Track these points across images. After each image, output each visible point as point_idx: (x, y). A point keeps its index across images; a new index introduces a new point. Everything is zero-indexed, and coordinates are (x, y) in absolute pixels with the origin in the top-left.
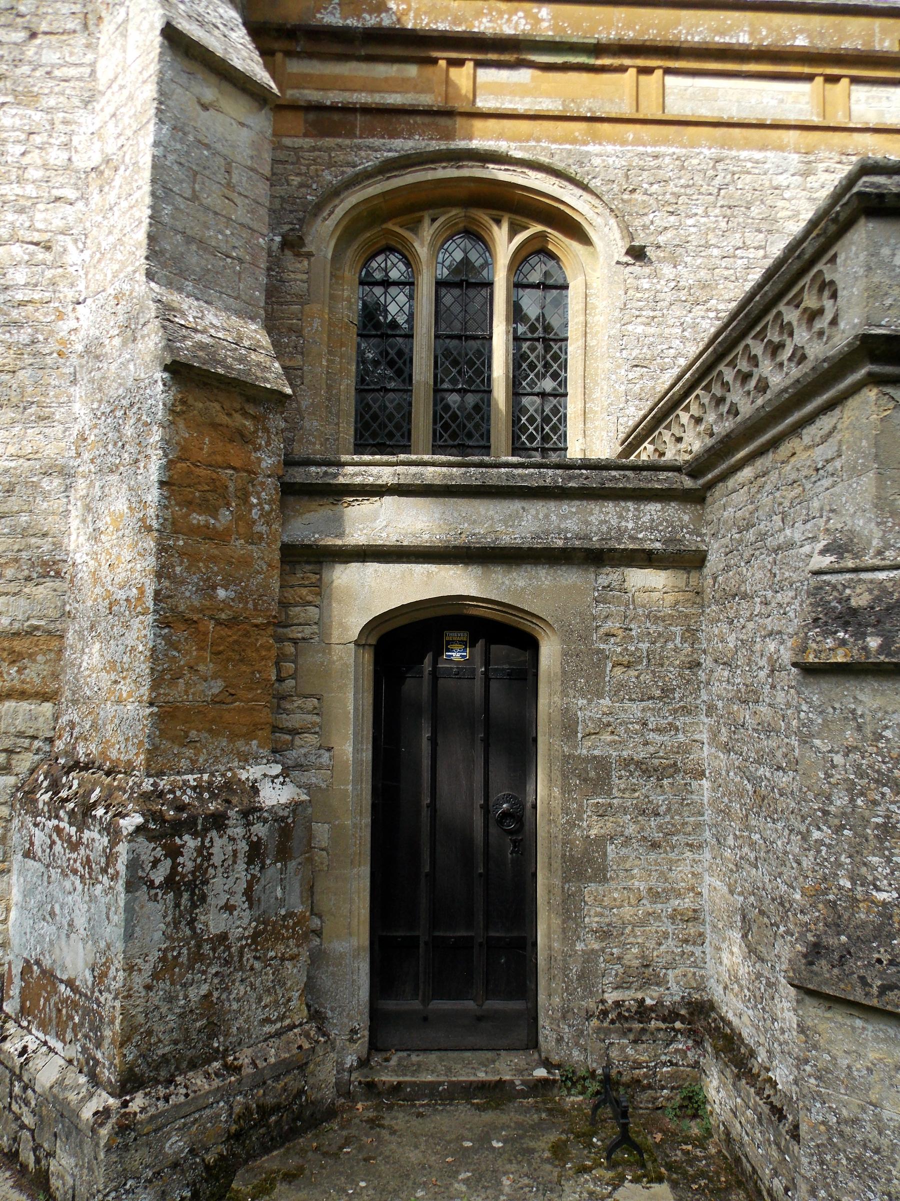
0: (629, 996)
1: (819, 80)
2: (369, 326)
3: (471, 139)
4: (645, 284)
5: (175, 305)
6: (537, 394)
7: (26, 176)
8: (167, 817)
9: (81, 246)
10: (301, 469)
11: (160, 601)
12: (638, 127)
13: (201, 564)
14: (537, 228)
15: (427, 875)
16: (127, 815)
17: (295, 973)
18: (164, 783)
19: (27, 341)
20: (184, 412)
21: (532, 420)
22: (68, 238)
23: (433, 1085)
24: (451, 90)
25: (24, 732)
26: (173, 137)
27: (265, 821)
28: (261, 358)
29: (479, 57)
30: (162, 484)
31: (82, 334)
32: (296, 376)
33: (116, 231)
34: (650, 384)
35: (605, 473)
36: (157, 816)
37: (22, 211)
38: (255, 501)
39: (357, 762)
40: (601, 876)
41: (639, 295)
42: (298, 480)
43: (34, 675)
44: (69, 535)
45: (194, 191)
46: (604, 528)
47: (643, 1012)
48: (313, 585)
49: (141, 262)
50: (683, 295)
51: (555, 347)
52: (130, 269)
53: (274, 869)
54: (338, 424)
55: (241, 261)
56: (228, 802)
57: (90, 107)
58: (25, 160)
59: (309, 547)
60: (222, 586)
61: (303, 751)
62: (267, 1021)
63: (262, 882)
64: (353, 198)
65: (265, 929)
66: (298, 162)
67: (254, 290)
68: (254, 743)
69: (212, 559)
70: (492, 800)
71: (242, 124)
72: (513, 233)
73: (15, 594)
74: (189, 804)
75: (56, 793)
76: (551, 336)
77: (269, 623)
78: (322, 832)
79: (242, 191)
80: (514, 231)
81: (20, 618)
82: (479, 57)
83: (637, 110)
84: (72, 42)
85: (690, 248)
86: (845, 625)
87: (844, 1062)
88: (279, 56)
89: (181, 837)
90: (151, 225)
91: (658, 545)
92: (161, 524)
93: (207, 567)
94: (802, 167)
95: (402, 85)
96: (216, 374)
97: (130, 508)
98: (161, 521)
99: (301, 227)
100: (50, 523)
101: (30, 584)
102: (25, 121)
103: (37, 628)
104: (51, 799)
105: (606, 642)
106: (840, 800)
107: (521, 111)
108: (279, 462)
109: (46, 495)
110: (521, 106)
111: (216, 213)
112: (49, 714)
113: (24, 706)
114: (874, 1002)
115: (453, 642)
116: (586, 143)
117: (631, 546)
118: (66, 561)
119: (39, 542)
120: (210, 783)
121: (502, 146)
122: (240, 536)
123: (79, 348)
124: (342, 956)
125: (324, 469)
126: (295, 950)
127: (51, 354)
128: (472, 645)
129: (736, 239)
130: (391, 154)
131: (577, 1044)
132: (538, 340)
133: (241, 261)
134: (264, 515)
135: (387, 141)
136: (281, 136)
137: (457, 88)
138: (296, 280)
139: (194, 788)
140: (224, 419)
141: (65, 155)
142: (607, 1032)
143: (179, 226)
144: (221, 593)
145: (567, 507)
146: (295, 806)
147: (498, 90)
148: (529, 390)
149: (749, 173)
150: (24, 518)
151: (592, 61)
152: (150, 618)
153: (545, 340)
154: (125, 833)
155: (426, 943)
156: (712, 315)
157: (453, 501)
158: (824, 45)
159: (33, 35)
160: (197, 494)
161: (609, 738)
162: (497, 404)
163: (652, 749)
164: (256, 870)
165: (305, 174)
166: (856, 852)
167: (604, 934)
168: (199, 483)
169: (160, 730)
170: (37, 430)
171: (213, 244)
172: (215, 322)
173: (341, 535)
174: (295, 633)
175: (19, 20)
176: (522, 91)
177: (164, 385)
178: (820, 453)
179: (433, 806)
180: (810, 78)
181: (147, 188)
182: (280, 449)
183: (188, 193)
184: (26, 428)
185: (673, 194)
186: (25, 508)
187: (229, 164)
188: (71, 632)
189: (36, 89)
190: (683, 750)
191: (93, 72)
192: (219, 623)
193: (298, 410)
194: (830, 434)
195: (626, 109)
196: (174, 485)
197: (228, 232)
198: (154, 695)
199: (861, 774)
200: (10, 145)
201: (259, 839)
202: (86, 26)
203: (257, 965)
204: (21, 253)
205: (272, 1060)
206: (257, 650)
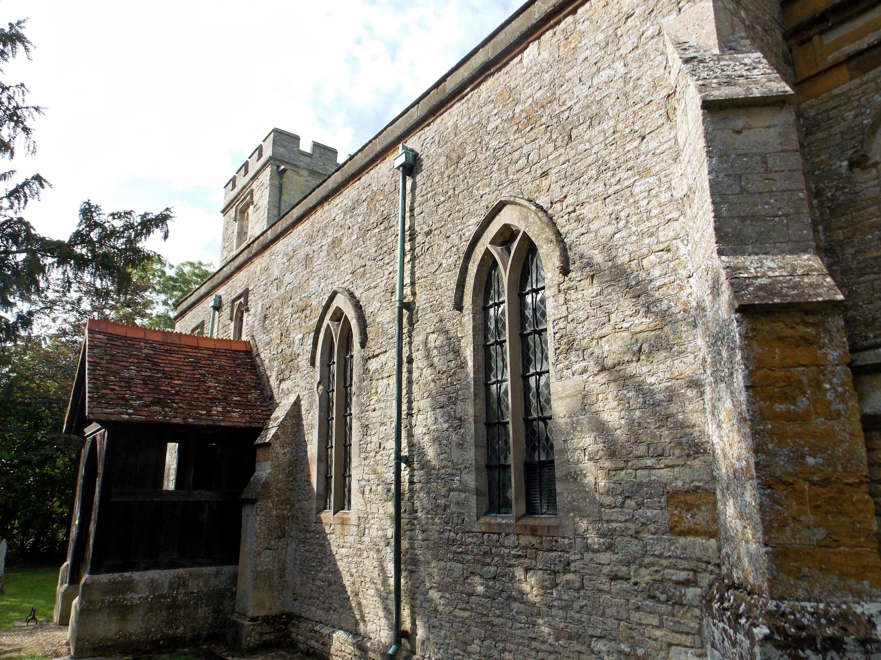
5: (740, 265)
8: (789, 633)
9: (685, 242)
10: (872, 352)
11: (761, 470)
13: (789, 440)
16: (758, 626)
18: (785, 606)
20: (755, 336)
22: (678, 241)
25: (701, 559)
26: (721, 163)
28: (814, 279)
30: (747, 388)
31: (694, 296)
33: (700, 230)
36: (782, 631)
37: (652, 235)
38: (828, 386)
42: (869, 362)
43: (701, 519)
44: (708, 424)
45: (741, 187)
49: (714, 247)
52: (710, 251)
56: (845, 630)
57: (678, 160)
58: (650, 205)
60: (810, 455)
68: (866, 583)
69: (798, 435)
71: (769, 127)
74: (808, 626)
75: (722, 604)
77: (861, 482)
79: (777, 169)
81: (688, 481)
84: (662, 131)
89: (803, 651)
90: (715, 222)
92: (752, 416)
93: (794, 442)
96: (775, 305)
97: (733, 405)
98: (751, 413)
99: (862, 147)
101: (691, 458)
102: (646, 185)
103: (698, 487)
104: (719, 607)
108: (845, 352)
111: (760, 193)
112: (715, 547)
113: (700, 540)
118: (708, 442)
120: (826, 612)
122: (818, 415)
123: (694, 304)
127: (680, 312)
133: (786, 215)
134: (837, 396)
136: (831, 90)
138: (868, 188)
139: (812, 614)
140: (788, 332)
143: (735, 214)
144: (810, 461)
152: (755, 482)
154: (757, 639)
159: (643, 138)
160: (776, 390)
168: (777, 382)
169: (776, 565)
170: (679, 361)
171: (762, 213)
172: (772, 265)
175: (636, 134)
177: (738, 322)
181: (709, 200)
182: (844, 342)
183: (737, 189)
184: (673, 361)
186: (680, 410)
187: (765, 157)
188: (718, 490)
191: (676, 141)
192: (812, 483)
196: (757, 387)
197: (772, 201)
198: (767, 538)
206: (854, 504)
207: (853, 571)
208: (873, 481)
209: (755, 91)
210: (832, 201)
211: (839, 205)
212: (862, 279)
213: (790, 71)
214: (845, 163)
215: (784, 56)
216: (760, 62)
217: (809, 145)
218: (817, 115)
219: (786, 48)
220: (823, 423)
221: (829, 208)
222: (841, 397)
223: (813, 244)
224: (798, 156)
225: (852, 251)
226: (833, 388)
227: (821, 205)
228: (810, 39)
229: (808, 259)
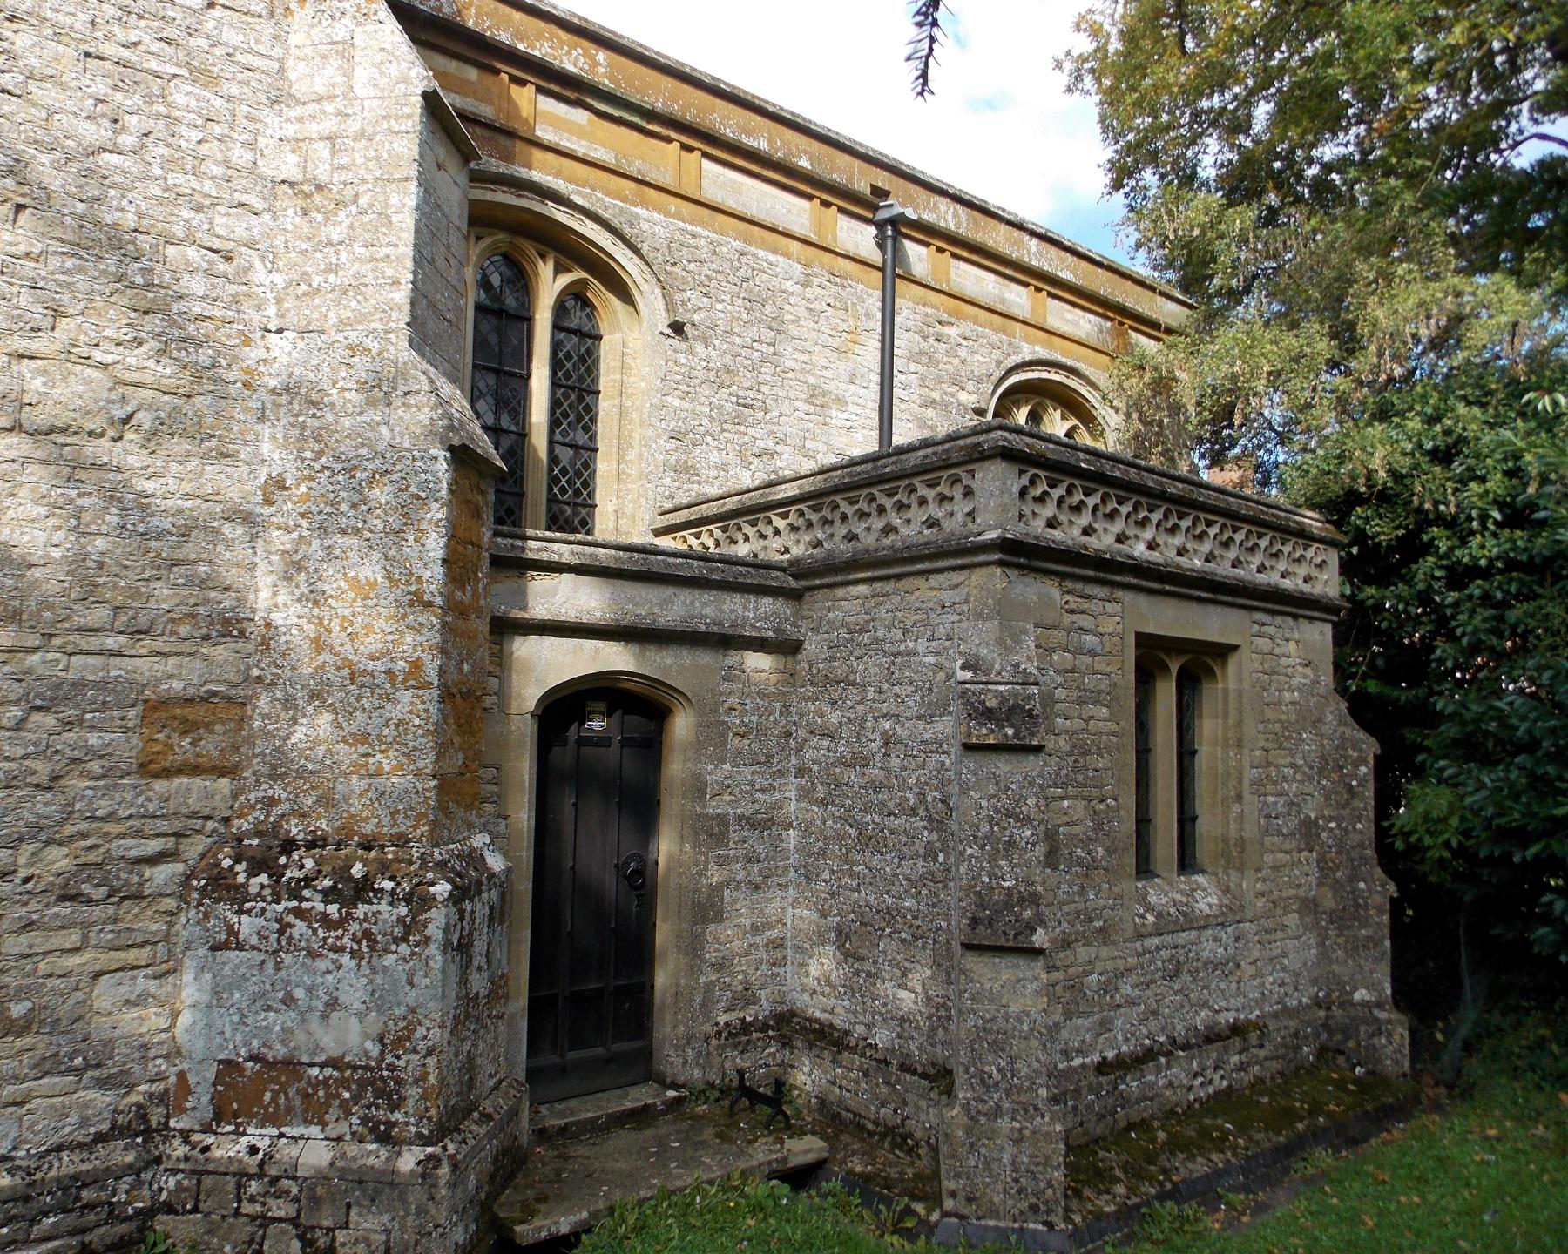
0: (733, 1016)
1: (817, 201)
3: (530, 168)
4: (682, 359)
6: (571, 446)
7: (203, 168)
9: (269, 265)
12: (679, 201)
14: (579, 274)
15: (569, 934)
19: (207, 364)
21: (564, 472)
29: (542, 84)
34: (684, 457)
37: (199, 209)
40: (719, 918)
47: (745, 1027)
51: (588, 399)
57: (276, 107)
58: (204, 149)
73: (190, 654)
82: (542, 84)
86: (989, 719)
87: (987, 986)
91: (770, 634)
100: (232, 576)
101: (206, 644)
103: (215, 694)
105: (729, 715)
106: (985, 828)
109: (229, 545)
110: (580, 148)
112: (226, 791)
113: (198, 782)
114: (1011, 944)
115: (594, 712)
119: (220, 597)
121: (560, 185)
128: (609, 716)
129: (753, 332)
132: (573, 388)
137: (517, 108)
141: (249, 156)
142: (723, 1047)
145: (708, 596)
147: (558, 123)
150: (203, 568)
151: (644, 124)
156: (734, 399)
157: (626, 583)
161: (728, 798)
162: (535, 450)
163: (757, 806)
166: (993, 859)
167: (720, 967)
170: (217, 468)
173: (524, 608)
176: (580, 133)
178: (947, 597)
180: (810, 198)
186: (205, 556)
189: (216, 70)
190: (778, 806)
194: (957, 586)
199: (997, 811)
200: (184, 127)
202: (272, 14)
204: (198, 259)
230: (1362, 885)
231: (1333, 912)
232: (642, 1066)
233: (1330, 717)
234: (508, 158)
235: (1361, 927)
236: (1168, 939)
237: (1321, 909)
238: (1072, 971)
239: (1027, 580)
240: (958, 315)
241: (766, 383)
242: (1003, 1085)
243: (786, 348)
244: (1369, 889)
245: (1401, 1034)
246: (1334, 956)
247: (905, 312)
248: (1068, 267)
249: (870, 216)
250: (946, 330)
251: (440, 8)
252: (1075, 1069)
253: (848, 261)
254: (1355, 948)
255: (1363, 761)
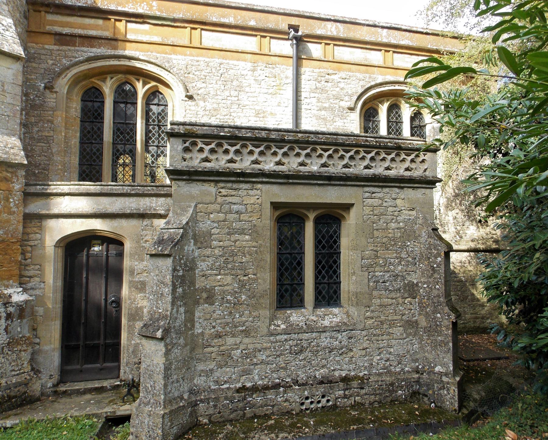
2: (86, 118)
10: (34, 187)
12: (191, 49)
14: (153, 84)
15: (83, 323)
17: (26, 356)
23: (78, 390)
24: (116, 31)
27: (13, 306)
32: (51, 140)
35: (146, 188)
38: (12, 200)
39: (55, 286)
41: (190, 112)
42: (32, 191)
46: (145, 206)
48: (38, 227)
50: (207, 113)
53: (17, 322)
54: (70, 157)
55: (8, 116)
59: (36, 214)
61: (34, 283)
62: (14, 370)
63: (12, 326)
64: (75, 71)
65: (13, 341)
66: (51, 55)
67: (14, 125)
68: (11, 281)
70: (109, 297)
71: (9, 68)
72: (143, 87)
76: (161, 124)
77: (18, 241)
78: (40, 310)
80: (144, 84)
83: (191, 43)
85: (210, 95)
88: (43, 13)
94: (252, 68)
95: (96, 27)
105: (146, 243)
107: (145, 41)
110: (145, 38)
116: (171, 54)
117: (153, 212)
122: (5, 213)
124: (47, 351)
125: (43, 187)
126: (26, 348)
128: (102, 245)
129: (227, 93)
130: (91, 54)
131: (131, 373)
133: (8, 116)
135: (89, 49)
136: (44, 44)
137: (119, 30)
138: (50, 102)
145: (132, 199)
146: (26, 302)
147: (136, 32)
148: (152, 144)
149: (232, 69)
151: (173, 24)
153: (158, 125)
155: (82, 346)
158: (260, 25)
161: (145, 274)
164: (9, 322)
165: (54, 60)
166: (157, 301)
174: (32, 243)
179: (86, 301)
185: (204, 75)
187: (3, 83)
193: (52, 153)
195: (186, 43)
197: (3, 107)
199: (158, 281)
201: (11, 312)
203: (9, 353)
205: (14, 382)
206: (13, 250)
207: (7, 277)
208: (23, 240)
209: (6, 47)
210: (33, 101)
211: (35, 104)
212: (39, 144)
213: (26, 22)
214: (43, 85)
215: (24, 13)
216: (11, 27)
217: (27, 67)
218: (35, 53)
219: (26, 9)
220: (6, 216)
221: (30, 104)
222: (17, 206)
223: (18, 133)
224: (20, 88)
225: (37, 129)
226: (14, 201)
227: (27, 100)
228: (40, 11)
229: (15, 140)
230: (439, 315)
231: (425, 328)
232: (115, 372)
233: (424, 234)
234: (116, 48)
235: (438, 336)
236: (293, 336)
237: (420, 326)
238: (222, 348)
239: (191, 185)
240: (339, 70)
241: (234, 112)
242: (152, 393)
243: (242, 96)
244: (442, 317)
245: (454, 390)
246: (426, 349)
247: (307, 73)
248: (406, 38)
249: (287, 37)
250: (333, 77)
251: (86, 3)
252: (223, 389)
253: (276, 57)
254: (435, 346)
255: (440, 255)
